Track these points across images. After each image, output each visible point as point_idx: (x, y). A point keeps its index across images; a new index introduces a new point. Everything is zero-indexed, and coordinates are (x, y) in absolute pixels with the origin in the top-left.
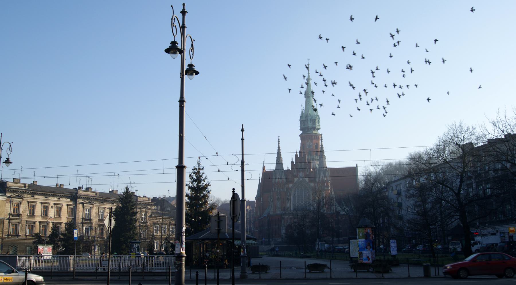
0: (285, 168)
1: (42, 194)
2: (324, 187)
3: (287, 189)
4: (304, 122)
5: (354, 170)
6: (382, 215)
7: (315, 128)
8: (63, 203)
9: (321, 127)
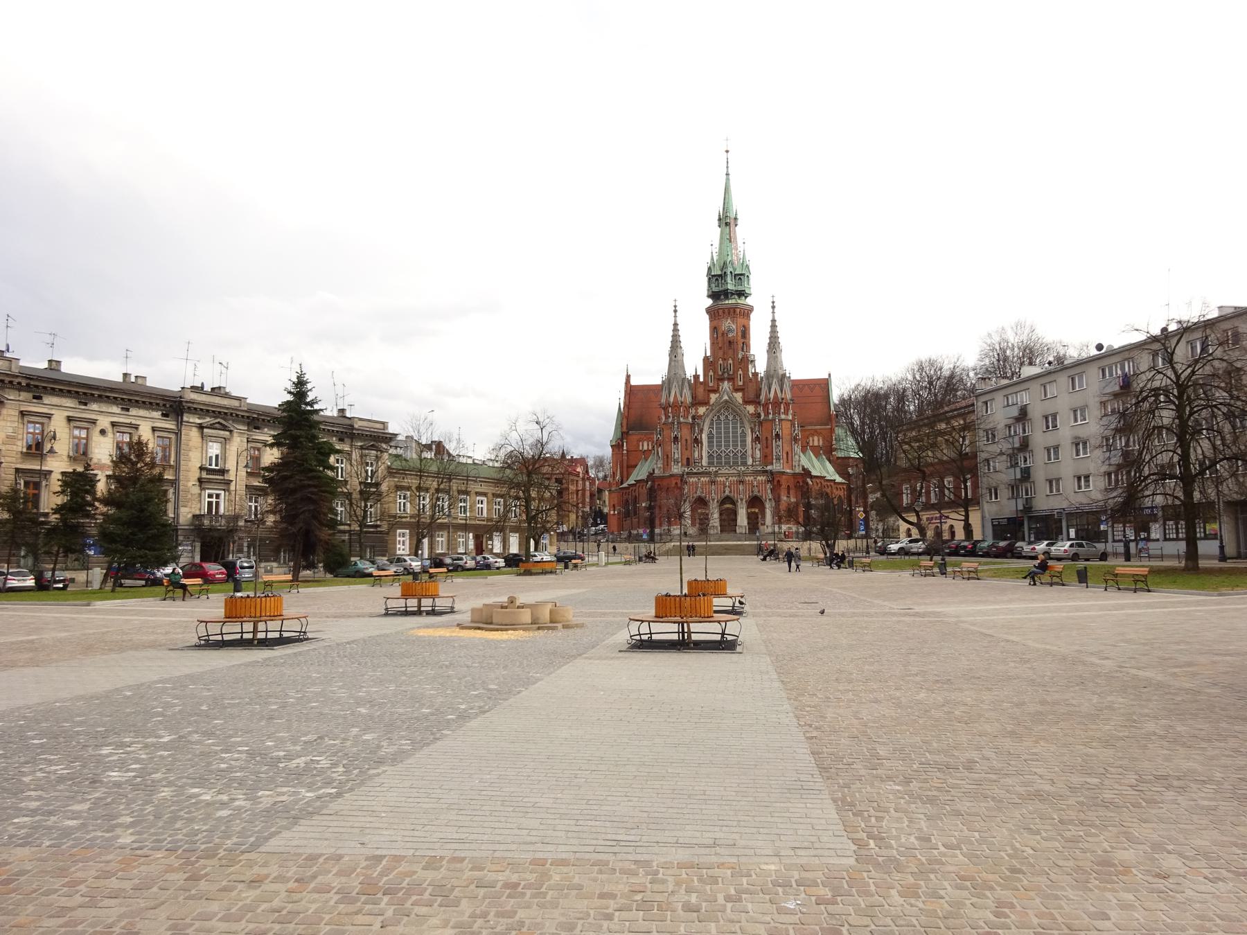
0: (690, 373)
1: (69, 392)
2: (779, 414)
3: (694, 418)
4: (717, 280)
5: (823, 386)
6: (641, 531)
7: (742, 294)
8: (138, 423)
9: (752, 291)
